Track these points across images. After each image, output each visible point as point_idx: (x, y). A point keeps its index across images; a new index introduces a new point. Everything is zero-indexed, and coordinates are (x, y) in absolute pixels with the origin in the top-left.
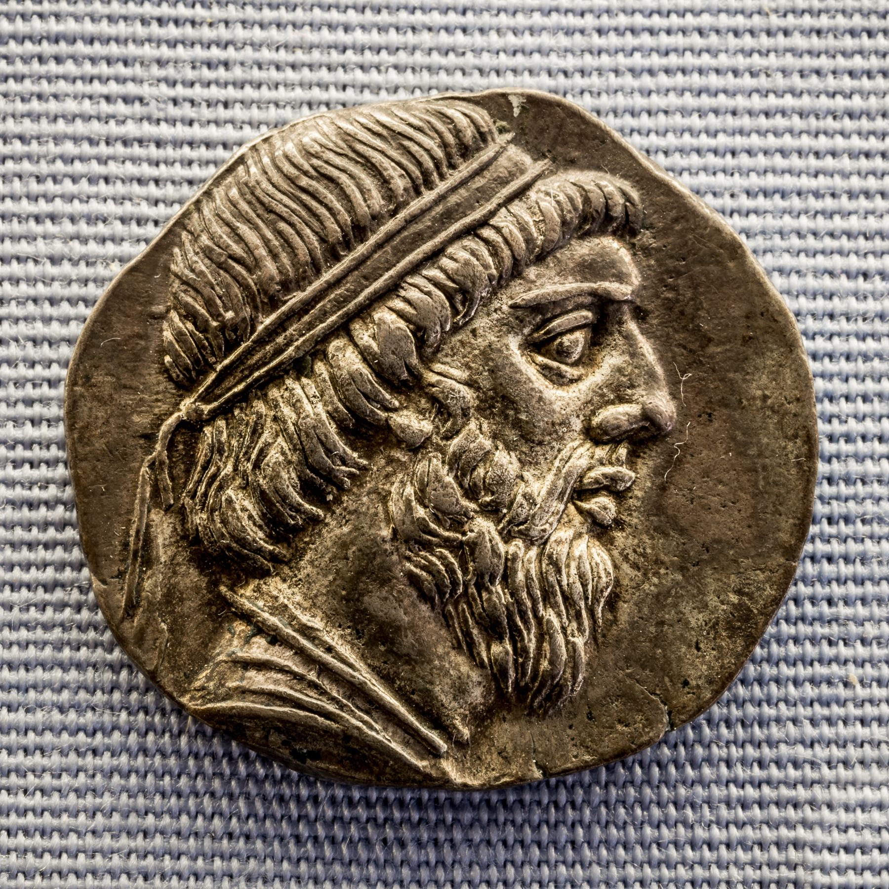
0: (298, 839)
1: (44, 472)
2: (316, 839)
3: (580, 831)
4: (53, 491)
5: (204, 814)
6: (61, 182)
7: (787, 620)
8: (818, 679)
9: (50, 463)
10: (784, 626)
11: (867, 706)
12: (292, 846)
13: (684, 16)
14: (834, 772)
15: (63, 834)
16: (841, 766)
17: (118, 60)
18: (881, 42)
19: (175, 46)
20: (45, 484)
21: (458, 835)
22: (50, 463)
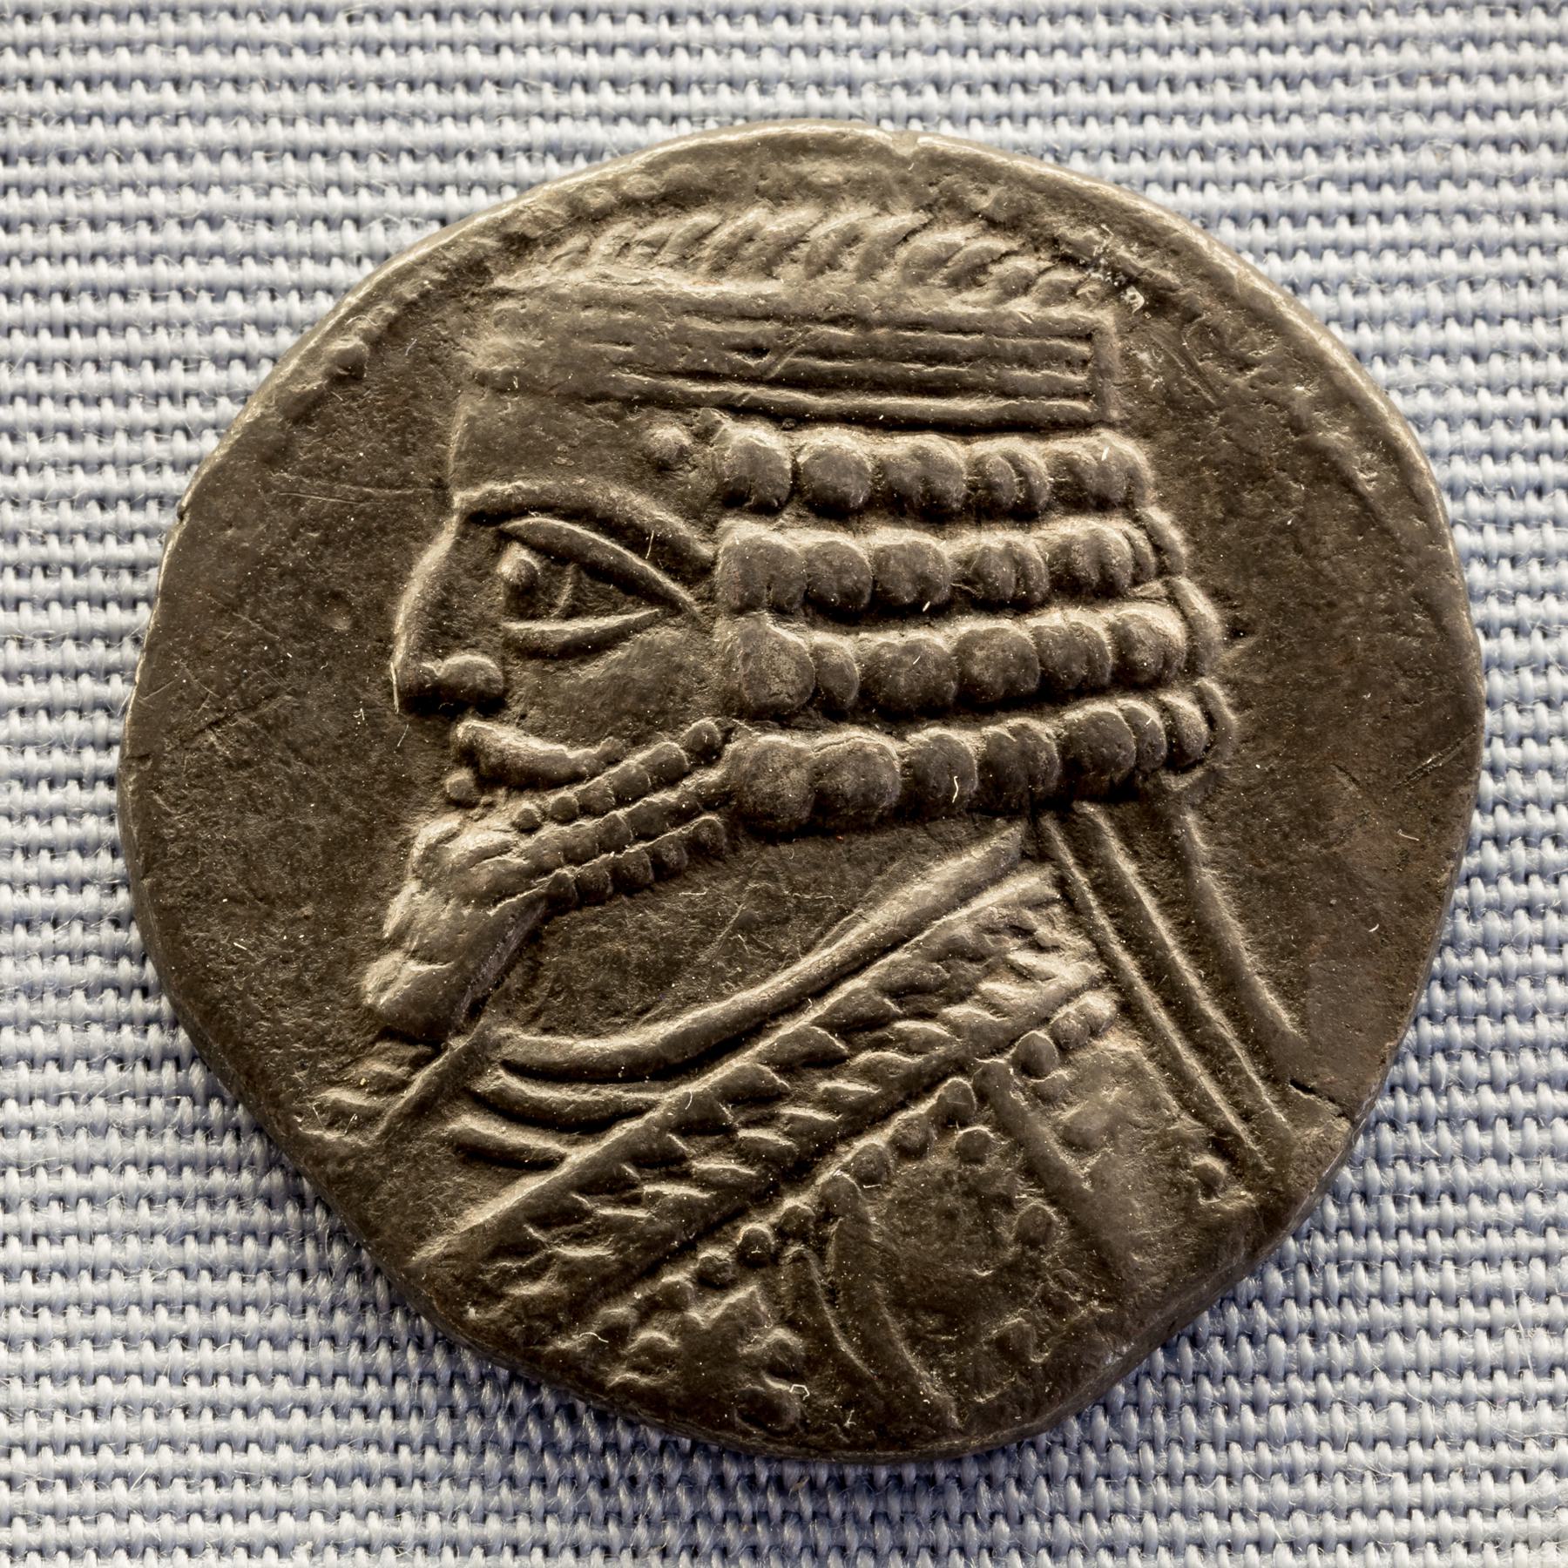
0: (604, 1484)
1: (75, 864)
2: (633, 1481)
3: (1090, 1456)
4: (91, 898)
5: (409, 1444)
6: (1123, 90)
7: (1431, 1016)
8: (1509, 906)
9: (84, 848)
10: (1426, 1027)
11: (1493, 1235)
12: (593, 1494)
13: (274, 1450)
14: (1417, 1487)
15: (123, 1447)
16: (1428, 1477)
17: (82, 289)
18: (1556, 368)
19: (95, 333)
20: (78, 885)
21: (852, 1537)
22: (84, 848)
